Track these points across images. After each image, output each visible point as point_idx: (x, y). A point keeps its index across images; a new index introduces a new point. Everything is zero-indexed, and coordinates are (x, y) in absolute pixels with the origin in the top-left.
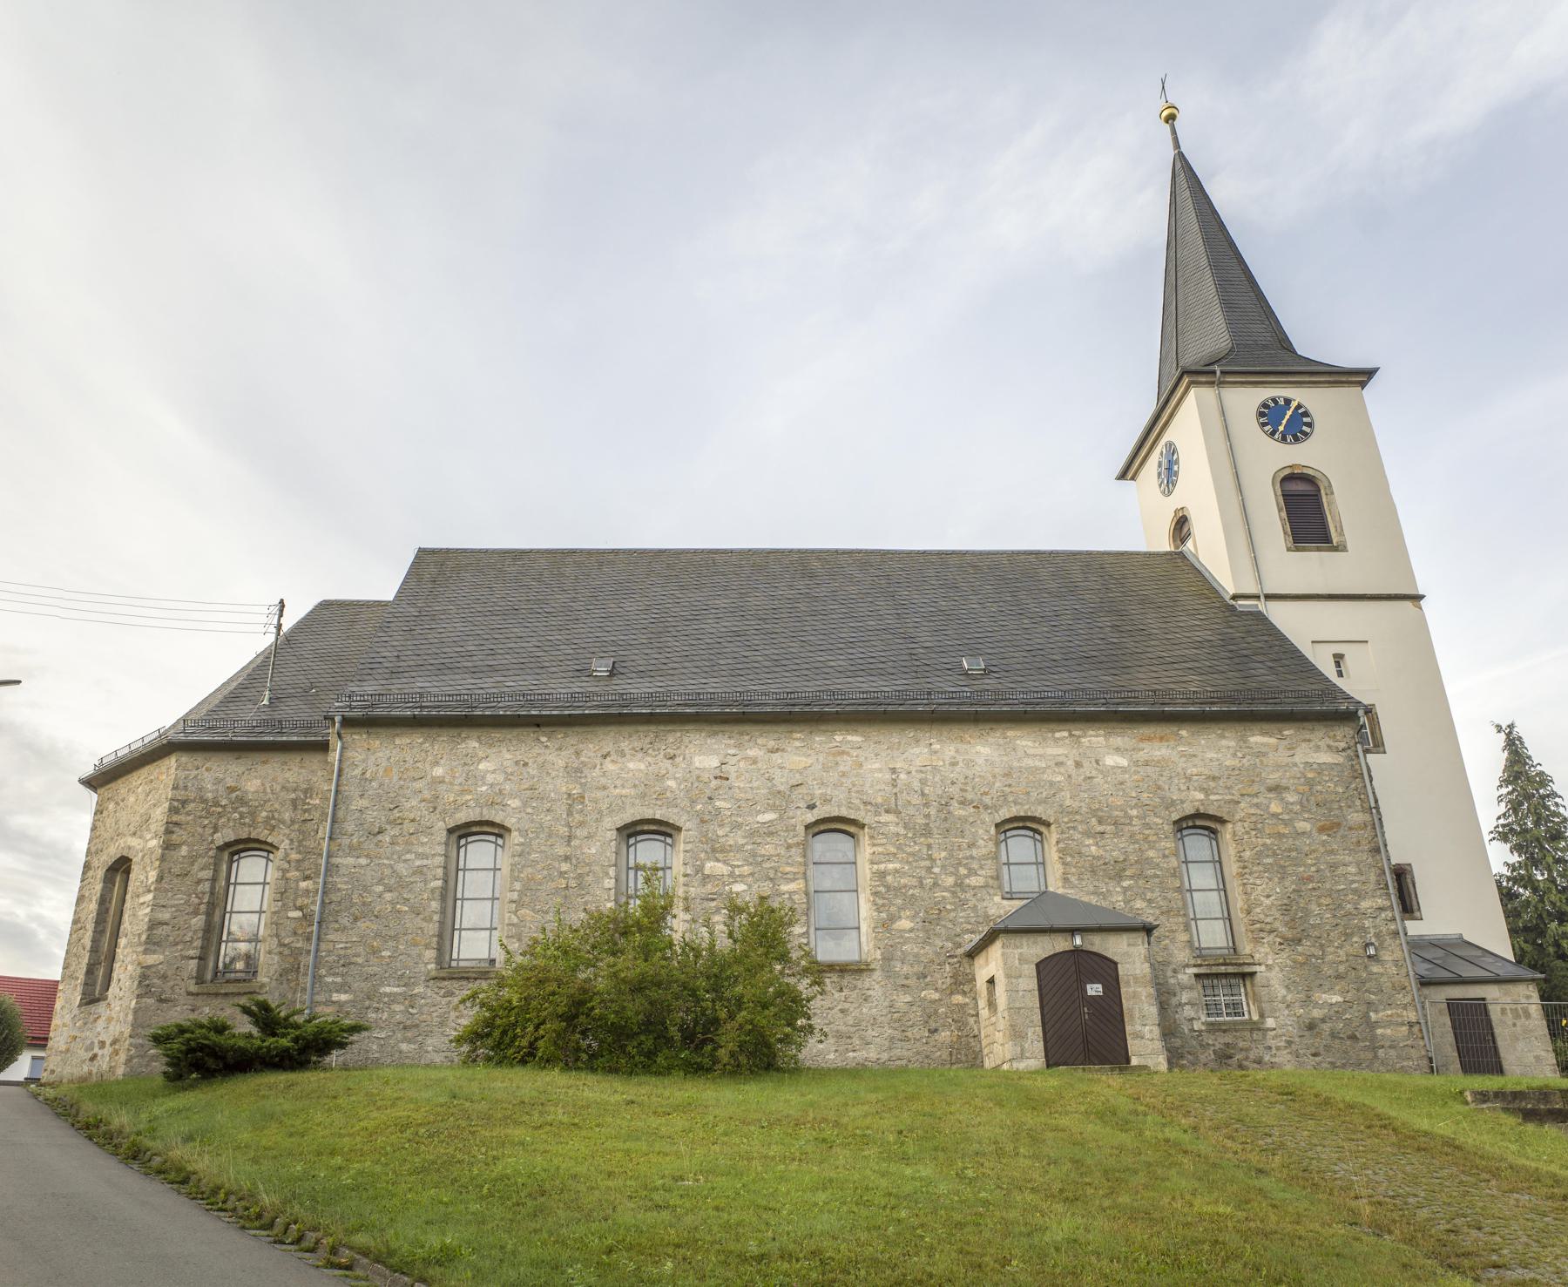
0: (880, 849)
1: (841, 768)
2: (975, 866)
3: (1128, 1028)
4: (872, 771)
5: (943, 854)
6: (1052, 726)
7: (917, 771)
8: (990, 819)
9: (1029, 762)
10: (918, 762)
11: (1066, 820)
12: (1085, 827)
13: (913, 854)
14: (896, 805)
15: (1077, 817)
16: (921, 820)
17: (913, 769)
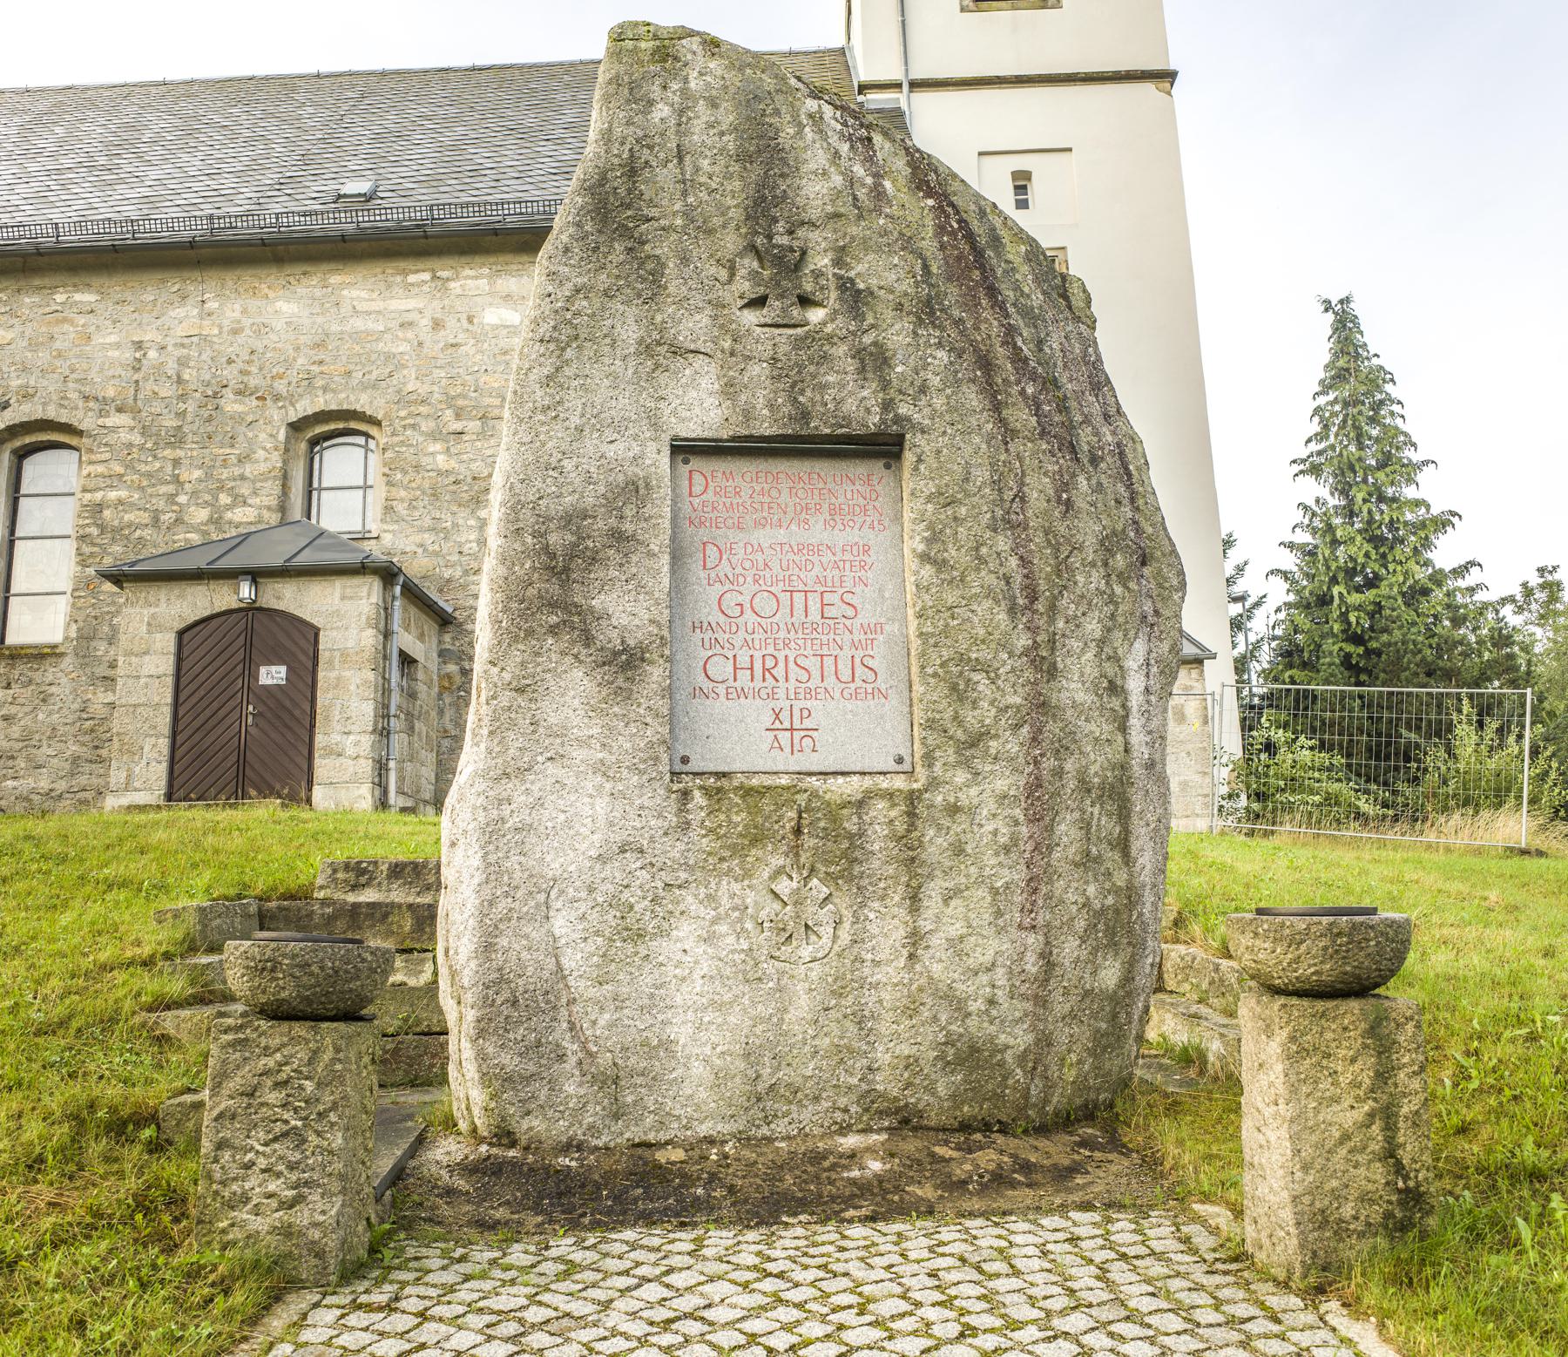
0: (100, 469)
1: (58, 345)
2: (245, 490)
3: (320, 740)
4: (104, 347)
5: (197, 474)
6: (402, 264)
7: (175, 345)
8: (278, 418)
9: (359, 324)
10: (180, 331)
11: (403, 413)
12: (432, 424)
13: (149, 475)
14: (135, 400)
15: (423, 409)
16: (170, 422)
17: (170, 341)
